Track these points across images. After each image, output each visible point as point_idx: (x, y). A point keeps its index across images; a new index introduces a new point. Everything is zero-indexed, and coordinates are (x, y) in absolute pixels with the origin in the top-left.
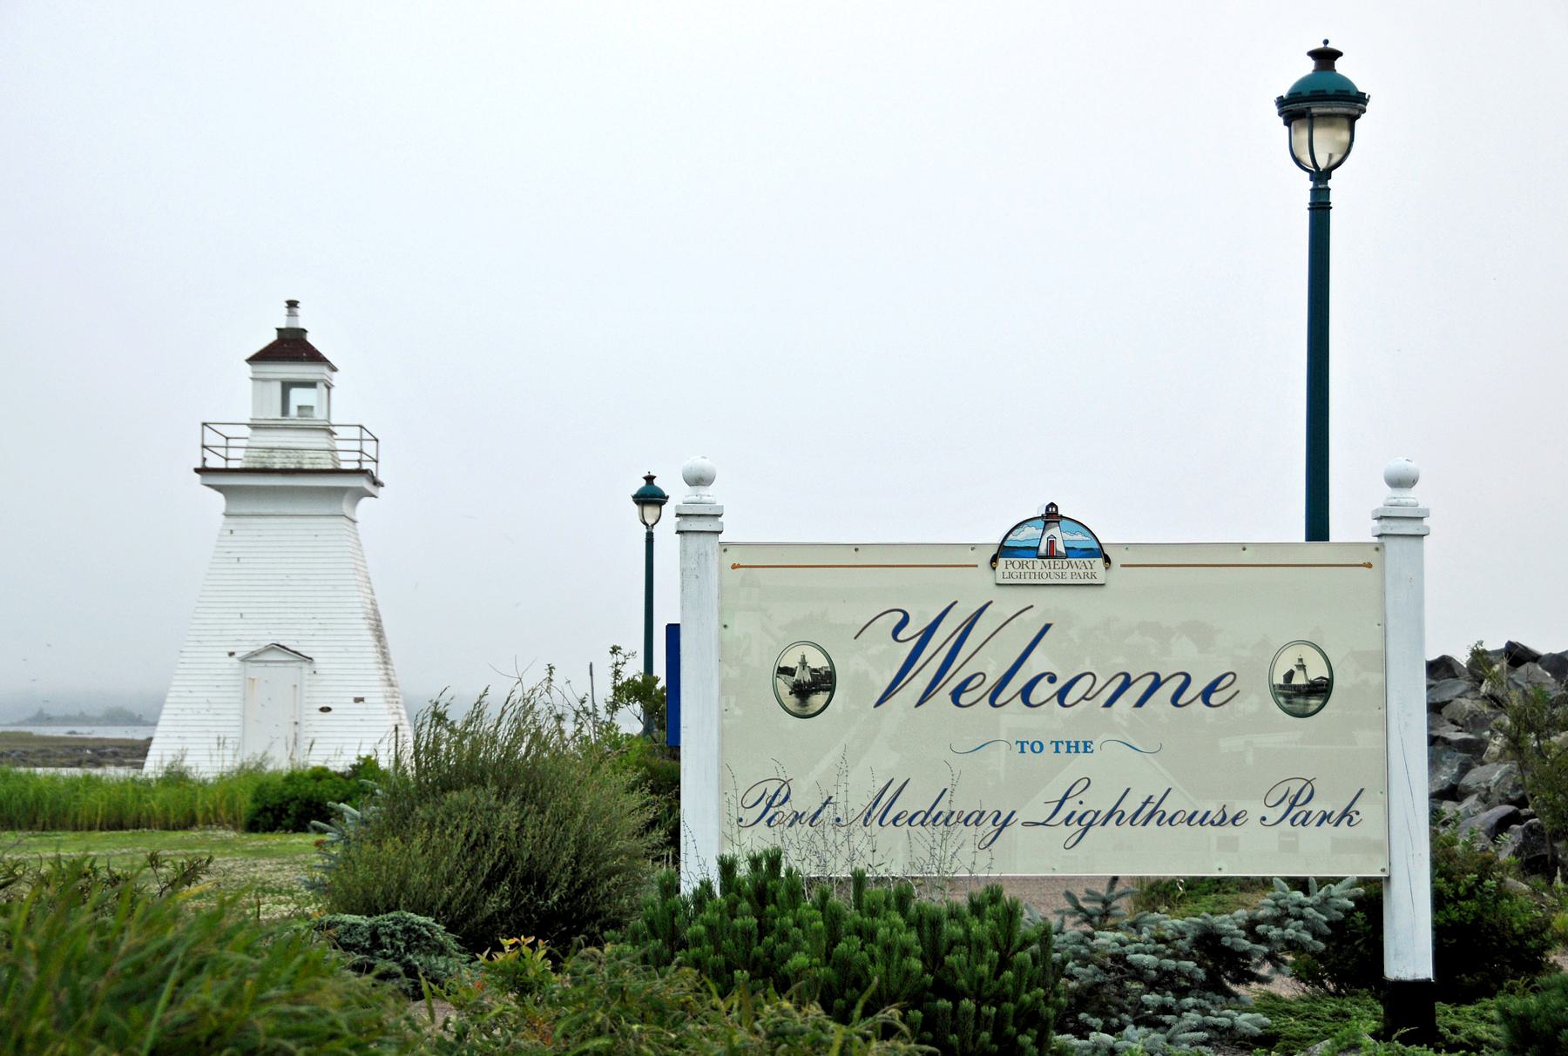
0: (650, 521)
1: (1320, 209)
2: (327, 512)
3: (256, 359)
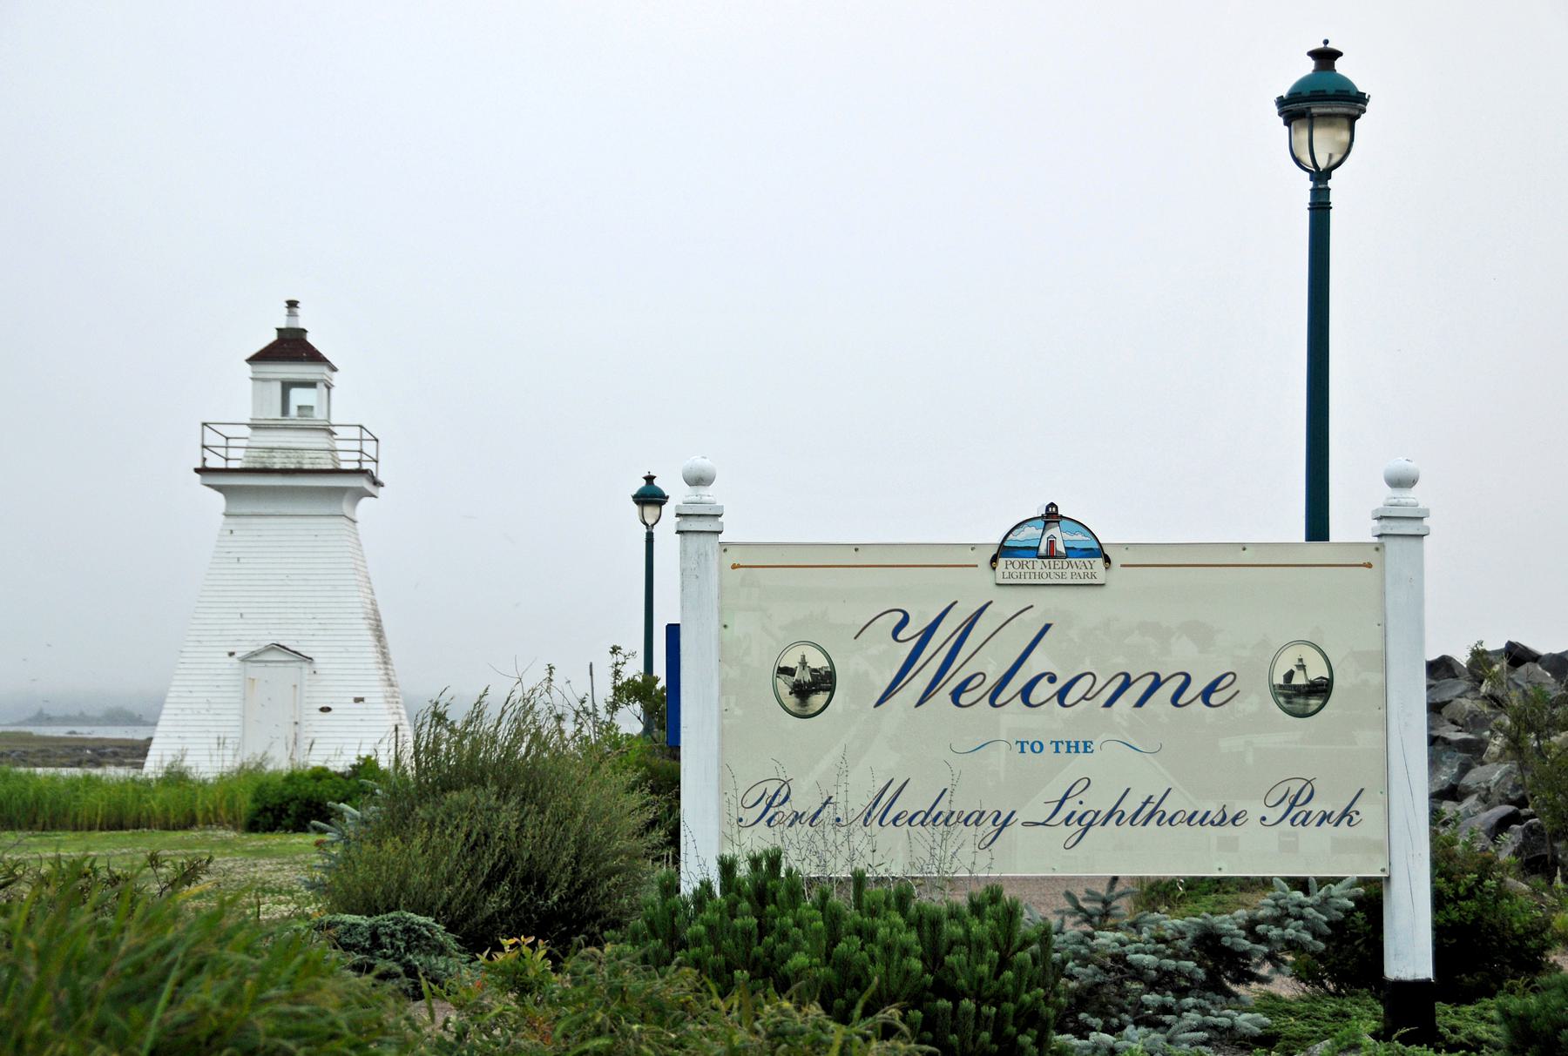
0: (650, 521)
1: (1320, 209)
2: (327, 511)
3: (256, 359)
